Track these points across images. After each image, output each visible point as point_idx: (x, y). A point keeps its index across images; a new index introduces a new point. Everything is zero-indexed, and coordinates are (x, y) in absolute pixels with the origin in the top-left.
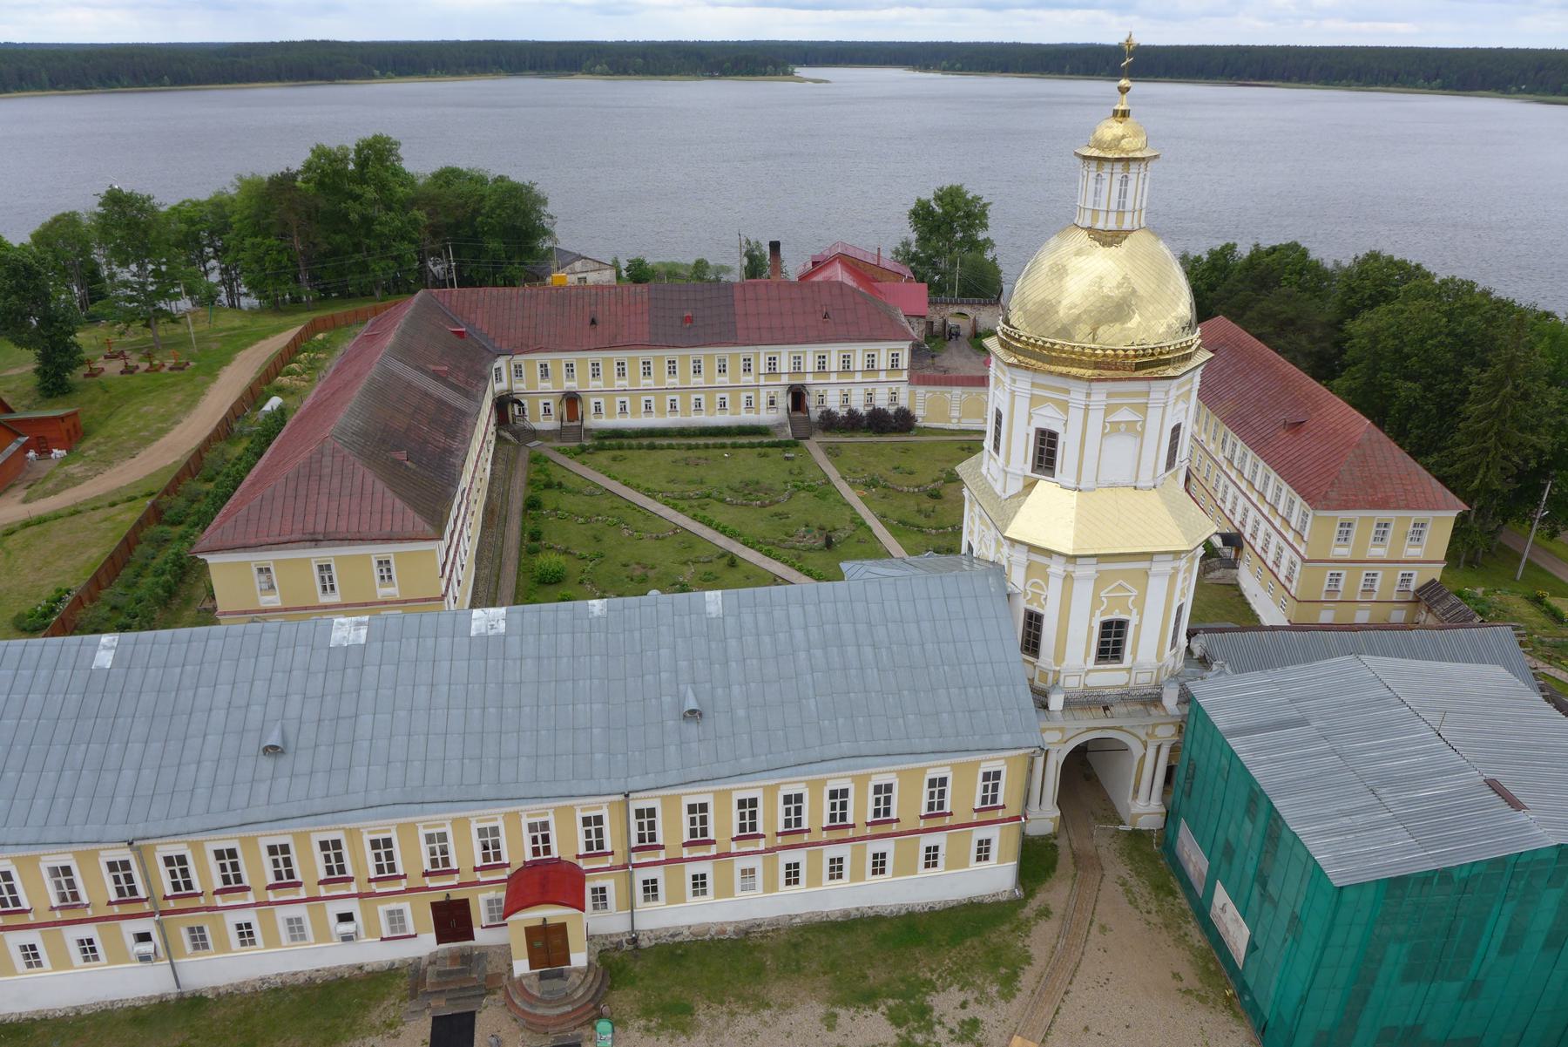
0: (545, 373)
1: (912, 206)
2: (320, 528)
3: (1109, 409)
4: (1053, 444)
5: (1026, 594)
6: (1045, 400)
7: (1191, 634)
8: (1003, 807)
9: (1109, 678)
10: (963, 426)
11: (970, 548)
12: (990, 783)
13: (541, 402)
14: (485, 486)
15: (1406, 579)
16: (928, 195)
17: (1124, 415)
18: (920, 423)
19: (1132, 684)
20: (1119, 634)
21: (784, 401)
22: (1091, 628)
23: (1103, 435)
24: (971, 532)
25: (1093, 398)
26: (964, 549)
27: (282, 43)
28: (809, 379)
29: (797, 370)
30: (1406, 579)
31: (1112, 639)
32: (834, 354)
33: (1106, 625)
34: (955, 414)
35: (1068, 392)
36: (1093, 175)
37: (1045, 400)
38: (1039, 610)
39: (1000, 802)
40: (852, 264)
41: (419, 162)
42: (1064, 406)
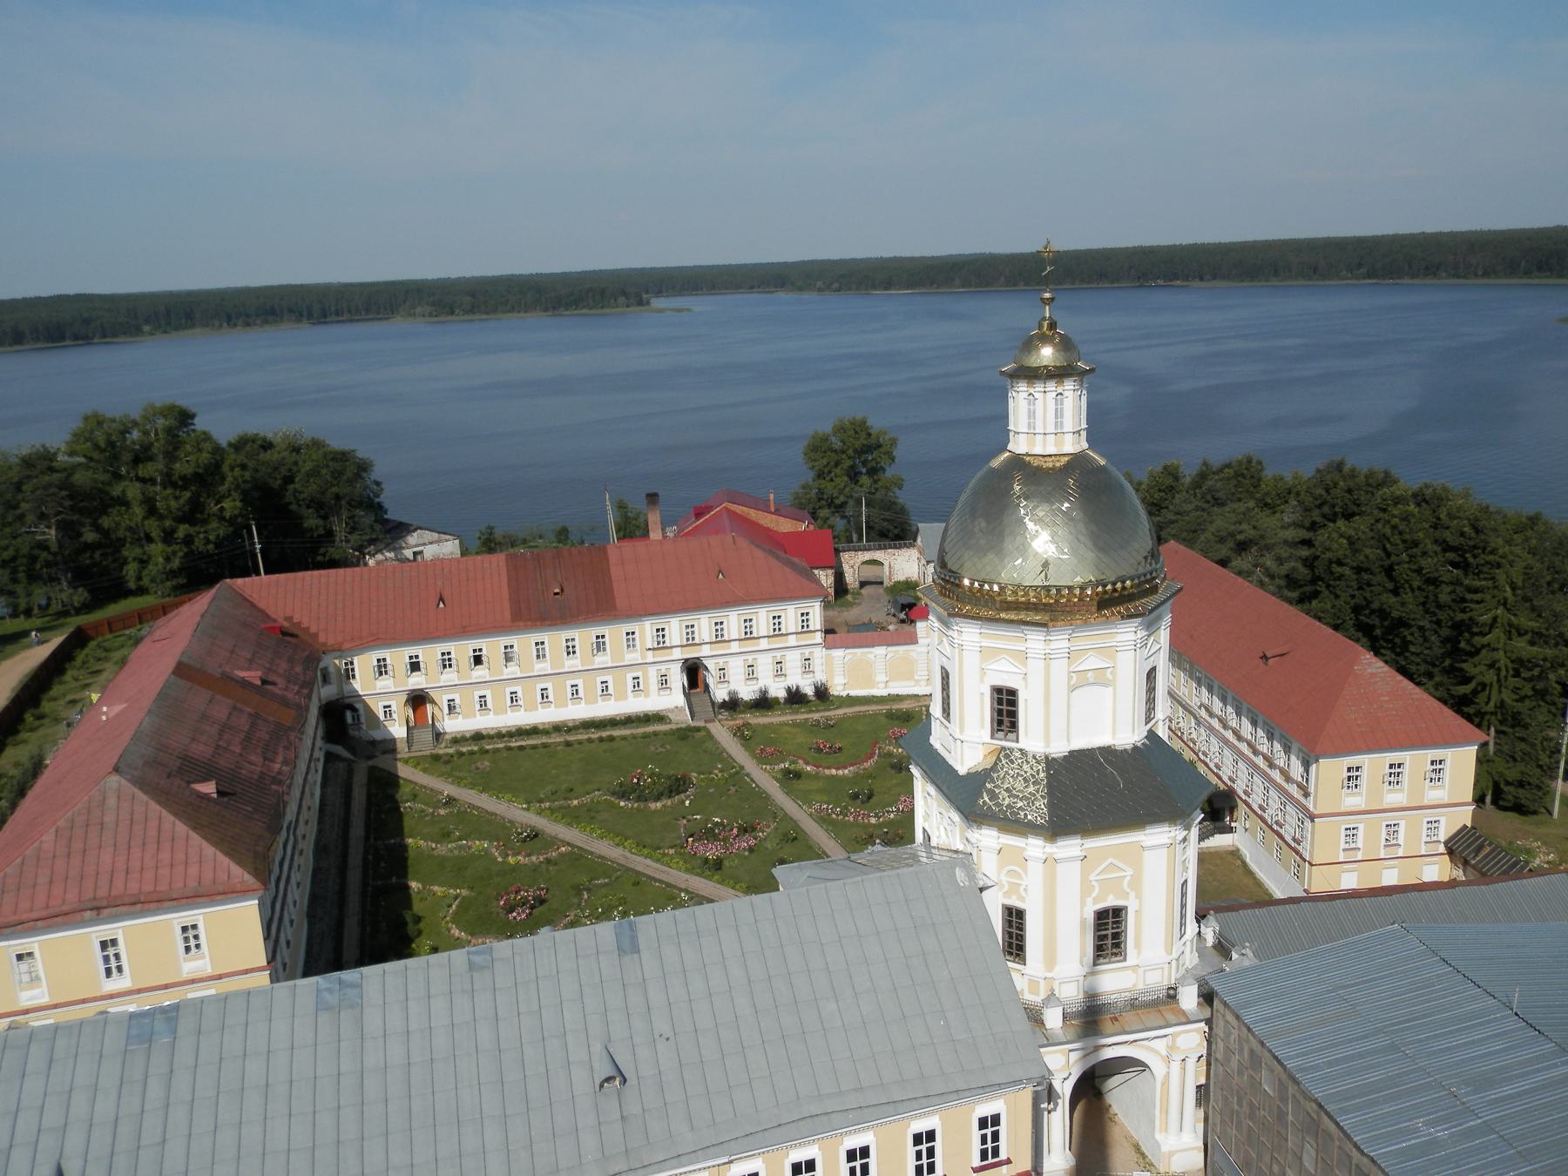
0: (571, 651)
2: (102, 892)
4: (1013, 703)
7: (1200, 917)
8: (1008, 1161)
10: (894, 691)
11: (927, 838)
12: (923, 1147)
13: (629, 676)
14: (314, 816)
17: (1092, 662)
19: (1141, 986)
21: (678, 679)
26: (919, 836)
27: (24, 299)
28: (705, 651)
29: (691, 642)
31: (1109, 932)
32: (733, 620)
34: (881, 678)
41: (221, 426)
42: (1023, 657)
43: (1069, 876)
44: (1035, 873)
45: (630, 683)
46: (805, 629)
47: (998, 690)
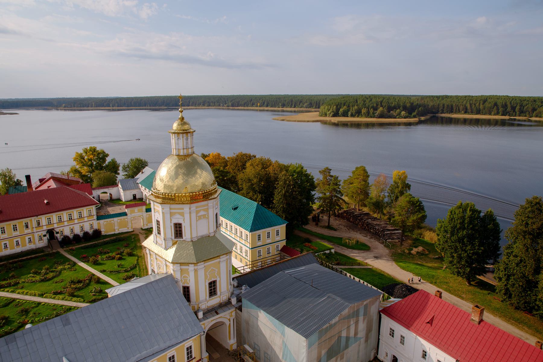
1: (74, 156)
3: (197, 212)
4: (181, 227)
5: (182, 281)
6: (175, 213)
8: (195, 358)
9: (215, 301)
11: (153, 271)
15: (277, 247)
16: (81, 151)
17: (202, 213)
18: (103, 233)
20: (214, 286)
22: (206, 286)
23: (197, 221)
24: (152, 265)
25: (192, 209)
29: (50, 223)
30: (277, 247)
32: (65, 215)
33: (210, 284)
35: (183, 209)
36: (185, 138)
37: (175, 213)
38: (188, 285)
39: (193, 357)
40: (55, 179)
42: (182, 214)
43: (201, 273)
44: (192, 274)
45: (27, 241)
46: (90, 215)
47: (176, 225)
